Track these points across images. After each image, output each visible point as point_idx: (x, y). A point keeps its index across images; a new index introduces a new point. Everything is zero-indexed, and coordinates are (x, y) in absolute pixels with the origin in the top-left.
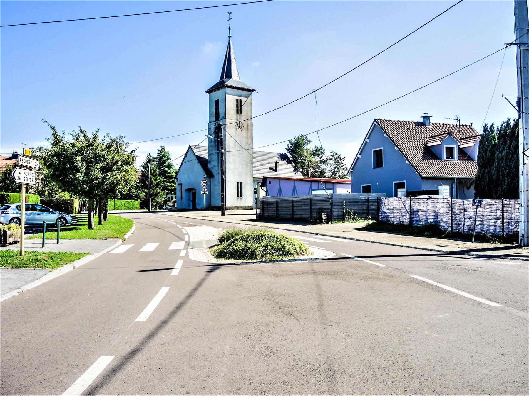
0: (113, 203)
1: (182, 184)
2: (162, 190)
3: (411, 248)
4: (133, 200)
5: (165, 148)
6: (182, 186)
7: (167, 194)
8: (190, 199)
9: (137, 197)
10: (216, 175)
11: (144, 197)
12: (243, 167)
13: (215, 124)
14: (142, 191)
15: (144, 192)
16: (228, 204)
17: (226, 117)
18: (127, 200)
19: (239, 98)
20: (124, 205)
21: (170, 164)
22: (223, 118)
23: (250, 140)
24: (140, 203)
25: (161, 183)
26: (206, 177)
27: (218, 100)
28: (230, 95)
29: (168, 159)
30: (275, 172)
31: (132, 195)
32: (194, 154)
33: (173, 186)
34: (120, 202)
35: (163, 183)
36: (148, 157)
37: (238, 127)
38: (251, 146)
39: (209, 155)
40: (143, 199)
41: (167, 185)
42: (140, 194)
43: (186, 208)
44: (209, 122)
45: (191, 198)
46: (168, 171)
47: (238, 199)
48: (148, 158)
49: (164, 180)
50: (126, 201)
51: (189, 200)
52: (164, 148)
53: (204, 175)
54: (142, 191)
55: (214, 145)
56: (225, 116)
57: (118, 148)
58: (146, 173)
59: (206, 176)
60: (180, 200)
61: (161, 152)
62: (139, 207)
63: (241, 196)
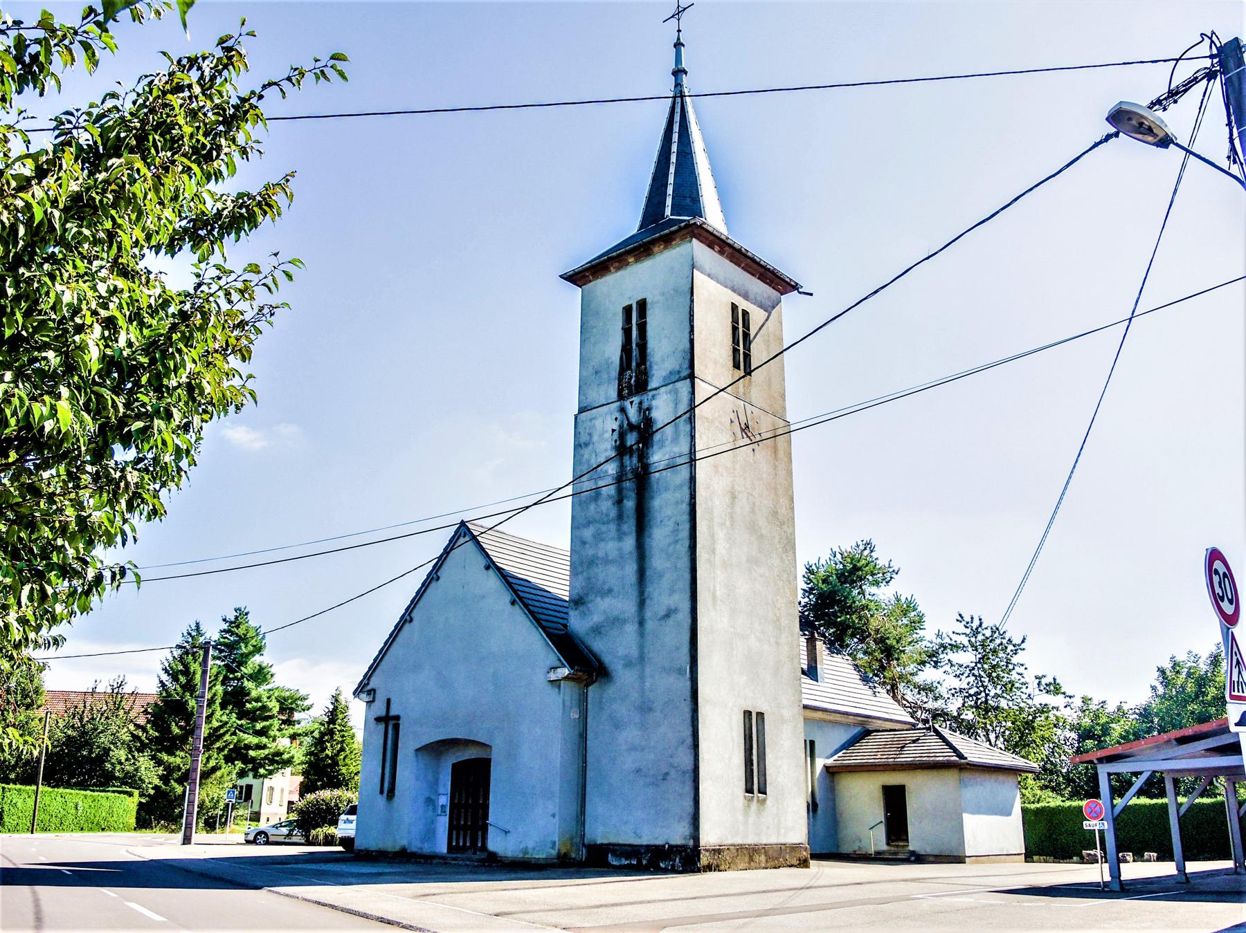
0: (31, 802)
1: (397, 718)
2: (229, 759)
3: (632, 901)
4: (114, 792)
5: (249, 615)
6: (397, 728)
7: (242, 774)
8: (433, 797)
9: (131, 781)
10: (628, 664)
11: (157, 782)
12: (763, 632)
13: (623, 410)
14: (153, 758)
15: (159, 763)
16: (710, 836)
17: (697, 373)
18: (88, 793)
19: (743, 304)
20: (73, 811)
21: (264, 669)
22: (676, 377)
23: (783, 501)
24: (140, 804)
25: (226, 732)
26: (566, 678)
27: (642, 305)
28: (709, 276)
29: (258, 649)
30: (815, 683)
31: (112, 772)
32: (491, 565)
33: (264, 747)
34: (59, 798)
35: (234, 734)
36: (189, 634)
37: (743, 430)
38: (790, 531)
39: (581, 562)
40: (153, 788)
41: (244, 740)
42: (143, 769)
43: (414, 849)
44: (582, 410)
45: (441, 790)
46: (254, 694)
47: (749, 806)
48: (190, 640)
49: (239, 722)
50: (86, 797)
51: (430, 802)
52: (247, 614)
53: (554, 668)
54: (151, 760)
55: (613, 513)
56: (686, 365)
57: (89, 744)
58: (178, 694)
59: (565, 671)
60: (381, 800)
61: (236, 623)
62: (133, 821)
63: (763, 791)
